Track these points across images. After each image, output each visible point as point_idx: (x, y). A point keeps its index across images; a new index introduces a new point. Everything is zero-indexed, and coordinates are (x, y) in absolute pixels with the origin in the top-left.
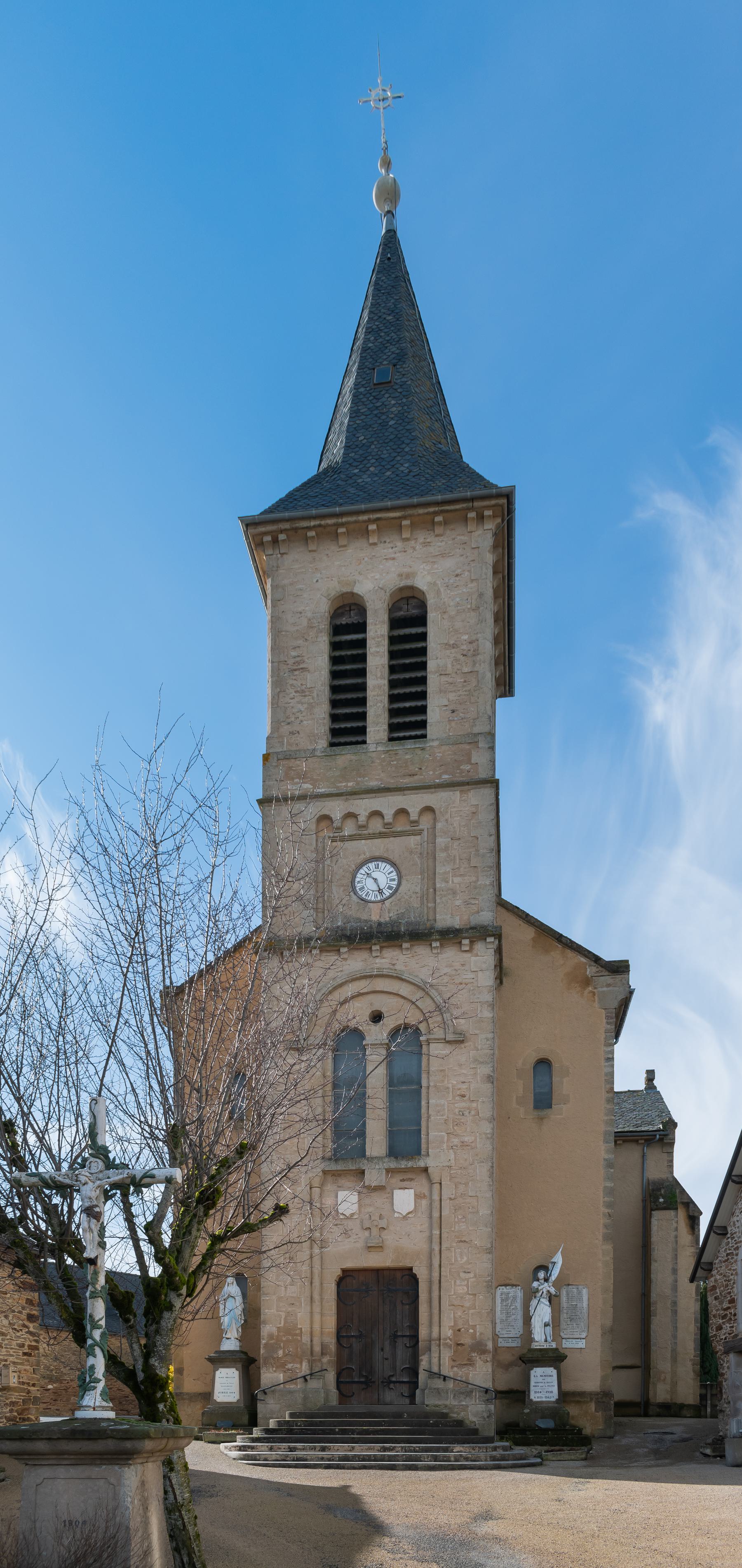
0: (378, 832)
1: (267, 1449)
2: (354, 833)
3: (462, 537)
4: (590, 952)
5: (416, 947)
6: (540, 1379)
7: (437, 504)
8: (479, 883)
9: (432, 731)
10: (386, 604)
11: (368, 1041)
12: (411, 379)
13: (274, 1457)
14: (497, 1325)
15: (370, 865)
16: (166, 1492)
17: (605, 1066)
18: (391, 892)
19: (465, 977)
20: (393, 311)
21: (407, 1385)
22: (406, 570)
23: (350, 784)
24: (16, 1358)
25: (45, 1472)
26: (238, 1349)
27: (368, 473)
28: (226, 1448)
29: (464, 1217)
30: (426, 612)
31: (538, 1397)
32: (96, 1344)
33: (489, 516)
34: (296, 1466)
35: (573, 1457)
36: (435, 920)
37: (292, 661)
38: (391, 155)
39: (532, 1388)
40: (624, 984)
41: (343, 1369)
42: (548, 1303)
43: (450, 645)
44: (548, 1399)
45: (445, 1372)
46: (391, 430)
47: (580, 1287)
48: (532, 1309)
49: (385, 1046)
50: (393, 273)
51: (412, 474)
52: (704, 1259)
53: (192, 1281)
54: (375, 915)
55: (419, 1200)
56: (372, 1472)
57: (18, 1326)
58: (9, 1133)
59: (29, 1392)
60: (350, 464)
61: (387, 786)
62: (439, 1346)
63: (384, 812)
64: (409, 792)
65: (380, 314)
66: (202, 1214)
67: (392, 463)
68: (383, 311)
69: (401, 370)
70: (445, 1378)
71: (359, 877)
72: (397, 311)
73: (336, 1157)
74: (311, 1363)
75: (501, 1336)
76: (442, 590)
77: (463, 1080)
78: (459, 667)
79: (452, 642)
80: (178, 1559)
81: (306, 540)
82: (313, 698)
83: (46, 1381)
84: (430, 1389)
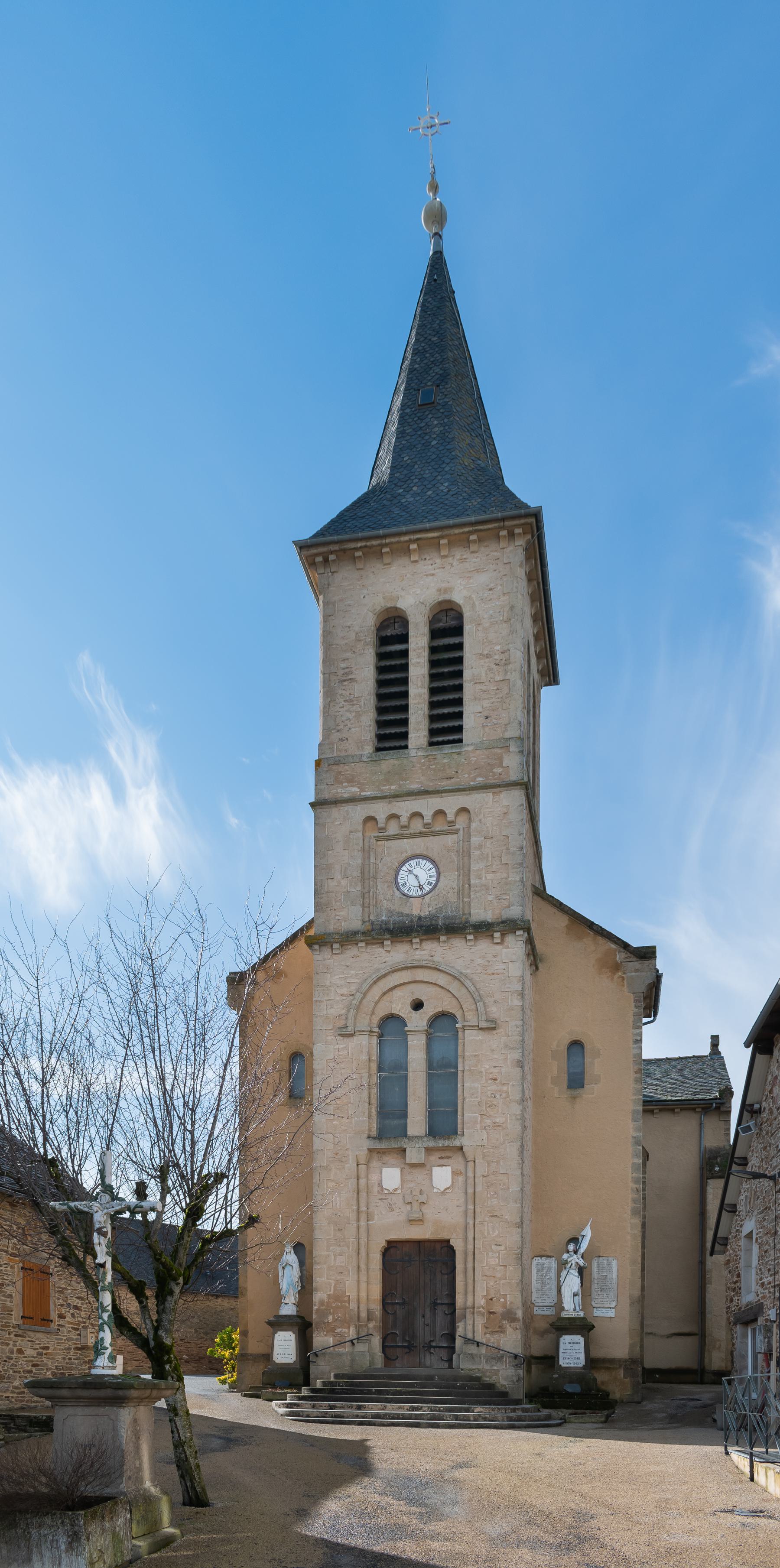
0: (418, 831)
1: (310, 1406)
2: (397, 833)
3: (495, 554)
4: (619, 939)
6: (569, 1346)
7: (471, 524)
8: (510, 879)
9: (467, 735)
10: (426, 616)
11: (410, 1027)
12: (453, 399)
13: (315, 1414)
15: (411, 862)
16: (172, 1432)
17: (634, 1048)
18: (430, 887)
19: (496, 967)
20: (437, 332)
21: (446, 1350)
22: (444, 585)
23: (393, 787)
25: (69, 1411)
26: (295, 1313)
27: (412, 492)
28: (276, 1405)
29: (496, 1193)
30: (463, 623)
31: (567, 1363)
32: (105, 1323)
33: (520, 534)
34: (333, 1423)
35: (593, 1420)
36: (470, 914)
37: (341, 672)
38: (438, 179)
39: (561, 1355)
40: (651, 969)
41: (389, 1334)
42: (577, 1274)
43: (483, 655)
44: (576, 1365)
45: (479, 1338)
46: (433, 450)
47: (610, 1259)
48: (562, 1279)
50: (439, 294)
51: (451, 493)
52: (720, 1234)
53: (187, 1273)
54: (416, 909)
56: (397, 1428)
58: (53, 1167)
60: (395, 484)
61: (427, 789)
62: (473, 1313)
63: (424, 814)
64: (446, 794)
65: (425, 336)
66: (190, 1225)
67: (433, 483)
68: (428, 332)
69: (444, 390)
70: (478, 1344)
71: (402, 874)
72: (442, 332)
73: (380, 1137)
74: (358, 1328)
76: (477, 603)
77: (495, 1064)
78: (492, 675)
79: (485, 652)
80: (184, 1484)
81: (354, 559)
82: (360, 707)
84: (465, 1353)
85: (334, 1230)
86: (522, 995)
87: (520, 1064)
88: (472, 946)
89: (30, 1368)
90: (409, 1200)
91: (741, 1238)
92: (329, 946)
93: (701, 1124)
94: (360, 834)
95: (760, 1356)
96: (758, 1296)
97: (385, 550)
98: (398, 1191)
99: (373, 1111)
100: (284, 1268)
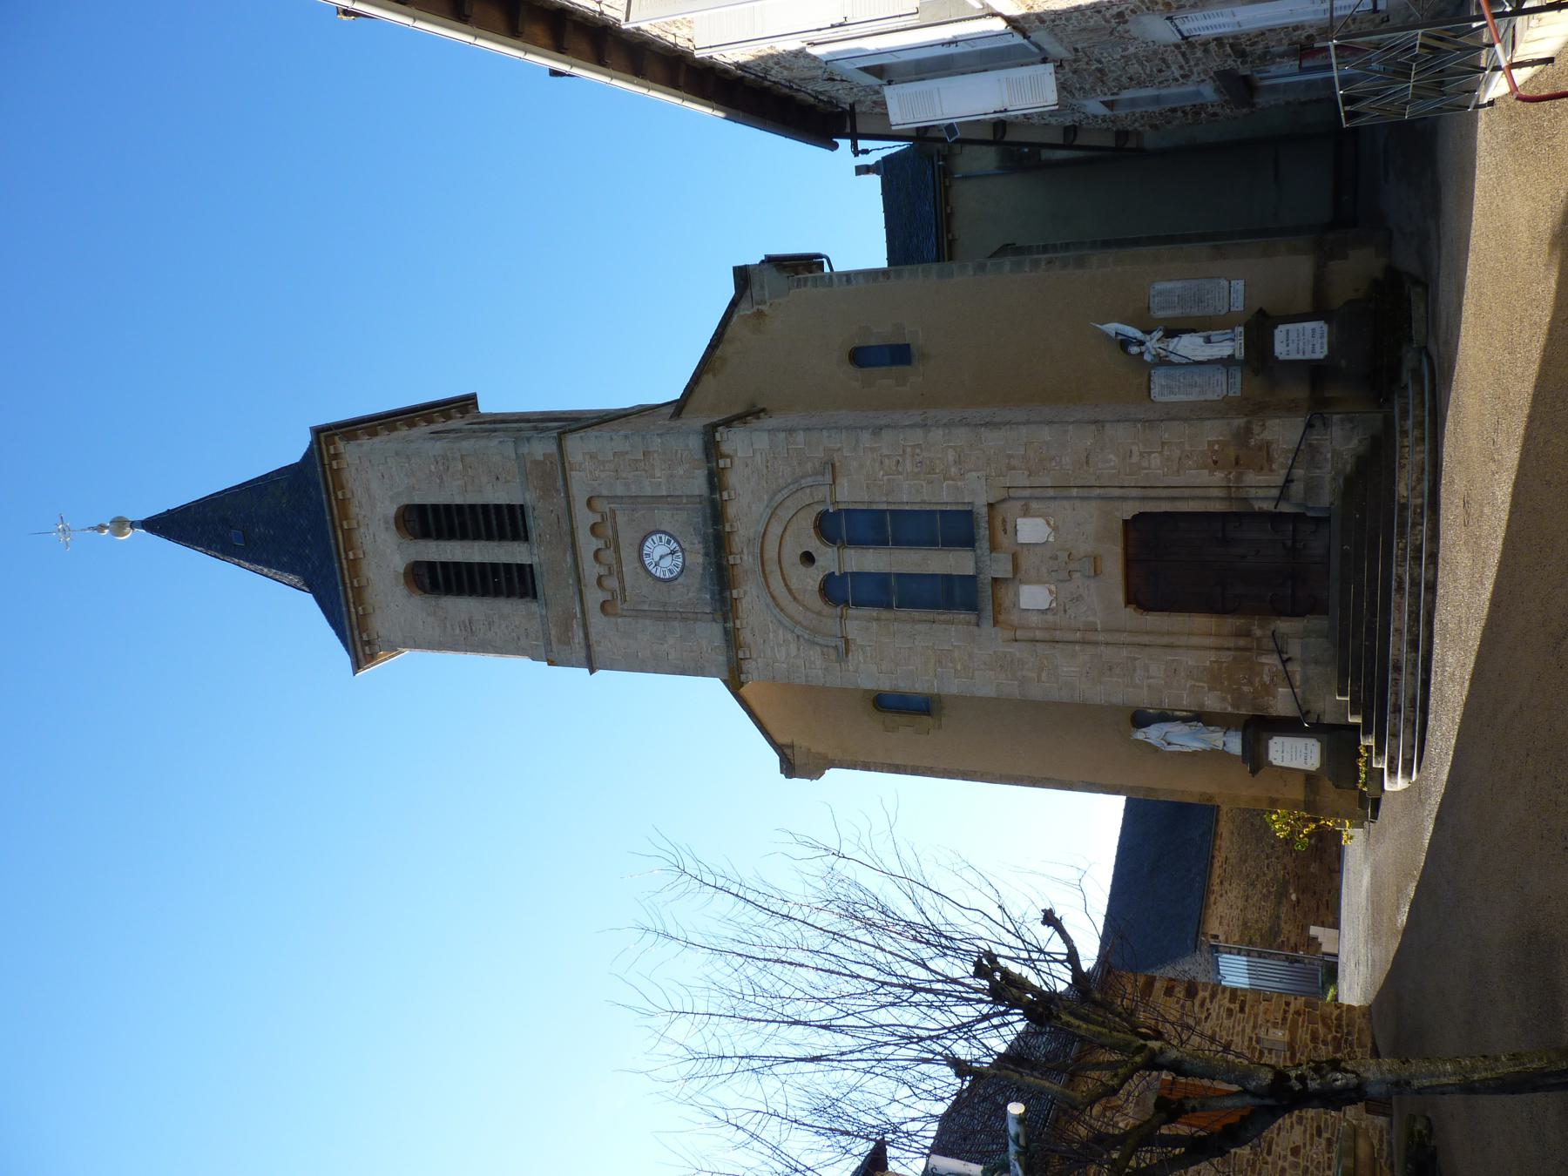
5: (729, 517)
6: (1293, 346)
10: (410, 542)
13: (1409, 731)
14: (1208, 399)
15: (646, 563)
18: (673, 541)
19: (759, 462)
24: (1247, 1023)
26: (1240, 734)
33: (335, 448)
39: (1307, 357)
42: (1176, 339)
43: (441, 482)
44: (1326, 334)
45: (1279, 479)
48: (1184, 361)
49: (841, 550)
54: (698, 559)
55: (1031, 511)
57: (1202, 1012)
59: (1297, 1013)
62: (1238, 487)
63: (595, 548)
70: (1289, 480)
74: (1262, 651)
75: (1225, 393)
83: (1284, 901)
86: (791, 431)
87: (877, 431)
88: (735, 493)
89: (1324, 1142)
91: (1114, 115)
92: (743, 662)
93: (966, 177)
94: (620, 620)
95: (1306, 64)
96: (1203, 81)
97: (356, 584)
99: (942, 617)
100: (1169, 744)
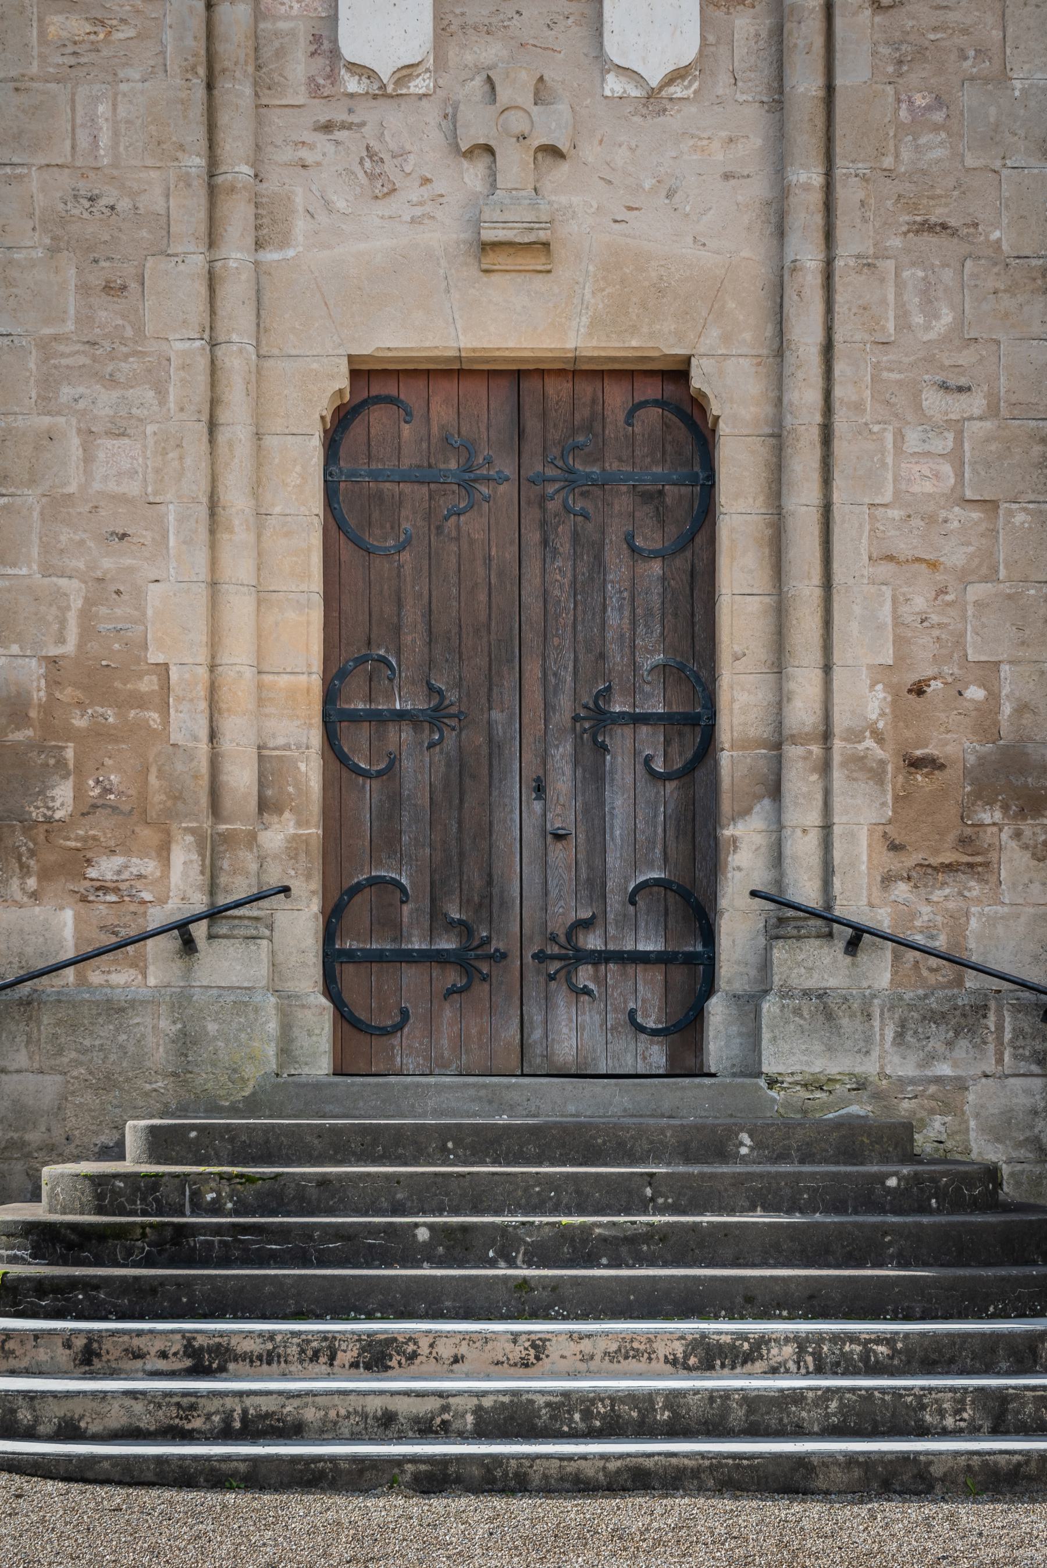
1: (63, 1356)
13: (116, 1419)
21: (657, 974)
29: (939, 101)
41: (356, 890)
55: (719, 14)
62: (825, 767)
84: (786, 993)
85: (84, 289)
90: (473, 134)
98: (420, 85)
